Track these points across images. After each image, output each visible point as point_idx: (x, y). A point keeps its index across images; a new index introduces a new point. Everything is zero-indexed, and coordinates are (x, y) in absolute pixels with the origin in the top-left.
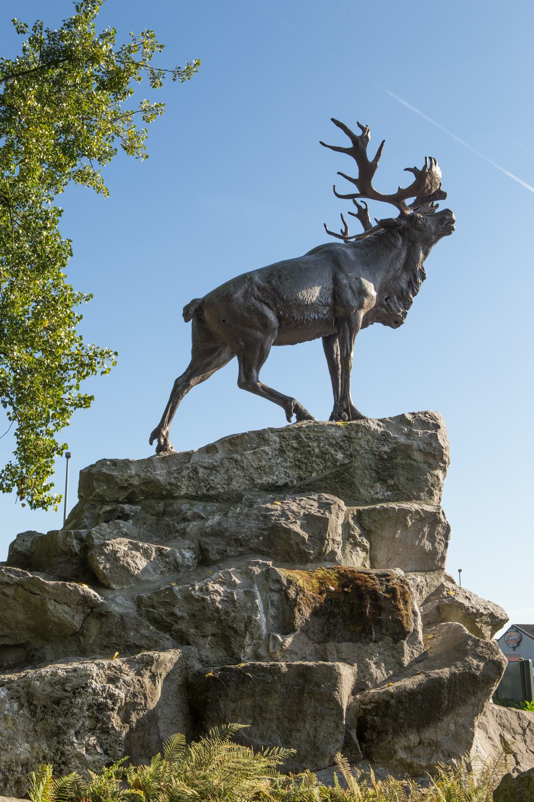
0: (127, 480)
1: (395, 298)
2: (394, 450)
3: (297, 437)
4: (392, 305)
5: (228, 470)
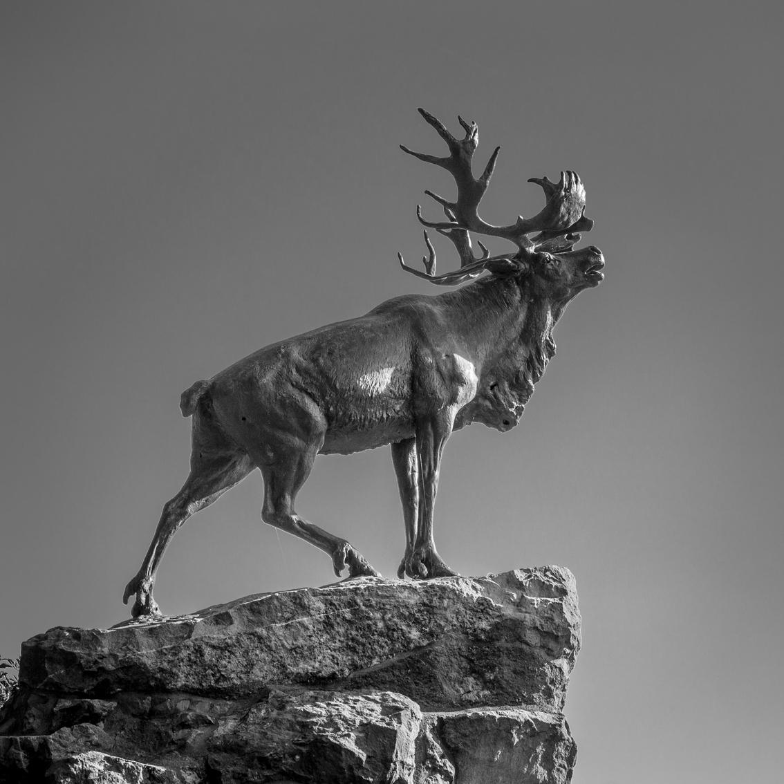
1: (506, 384)
2: (496, 627)
3: (351, 604)
4: (500, 396)
5: (247, 652)
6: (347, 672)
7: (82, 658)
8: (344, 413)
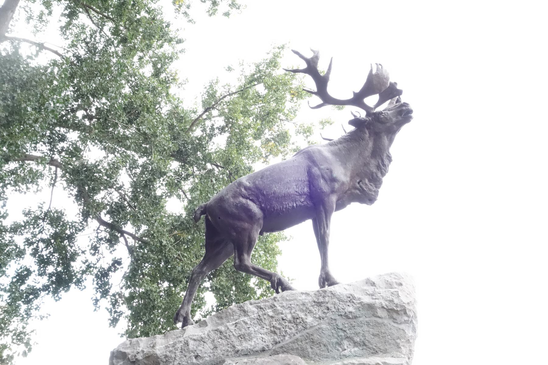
0: (135, 356)
1: (367, 181)
4: (364, 187)
5: (213, 341)
6: (271, 346)
7: (129, 354)
8: (270, 207)
